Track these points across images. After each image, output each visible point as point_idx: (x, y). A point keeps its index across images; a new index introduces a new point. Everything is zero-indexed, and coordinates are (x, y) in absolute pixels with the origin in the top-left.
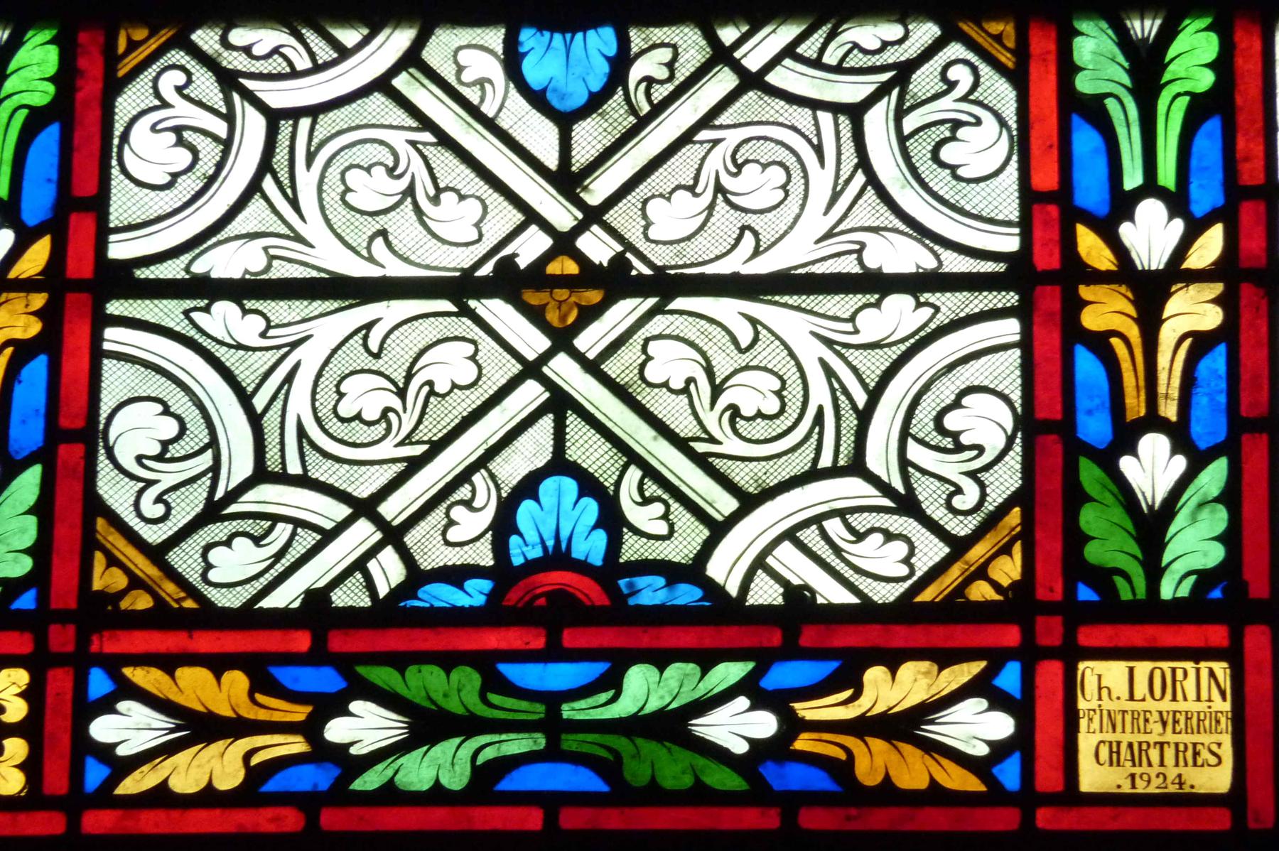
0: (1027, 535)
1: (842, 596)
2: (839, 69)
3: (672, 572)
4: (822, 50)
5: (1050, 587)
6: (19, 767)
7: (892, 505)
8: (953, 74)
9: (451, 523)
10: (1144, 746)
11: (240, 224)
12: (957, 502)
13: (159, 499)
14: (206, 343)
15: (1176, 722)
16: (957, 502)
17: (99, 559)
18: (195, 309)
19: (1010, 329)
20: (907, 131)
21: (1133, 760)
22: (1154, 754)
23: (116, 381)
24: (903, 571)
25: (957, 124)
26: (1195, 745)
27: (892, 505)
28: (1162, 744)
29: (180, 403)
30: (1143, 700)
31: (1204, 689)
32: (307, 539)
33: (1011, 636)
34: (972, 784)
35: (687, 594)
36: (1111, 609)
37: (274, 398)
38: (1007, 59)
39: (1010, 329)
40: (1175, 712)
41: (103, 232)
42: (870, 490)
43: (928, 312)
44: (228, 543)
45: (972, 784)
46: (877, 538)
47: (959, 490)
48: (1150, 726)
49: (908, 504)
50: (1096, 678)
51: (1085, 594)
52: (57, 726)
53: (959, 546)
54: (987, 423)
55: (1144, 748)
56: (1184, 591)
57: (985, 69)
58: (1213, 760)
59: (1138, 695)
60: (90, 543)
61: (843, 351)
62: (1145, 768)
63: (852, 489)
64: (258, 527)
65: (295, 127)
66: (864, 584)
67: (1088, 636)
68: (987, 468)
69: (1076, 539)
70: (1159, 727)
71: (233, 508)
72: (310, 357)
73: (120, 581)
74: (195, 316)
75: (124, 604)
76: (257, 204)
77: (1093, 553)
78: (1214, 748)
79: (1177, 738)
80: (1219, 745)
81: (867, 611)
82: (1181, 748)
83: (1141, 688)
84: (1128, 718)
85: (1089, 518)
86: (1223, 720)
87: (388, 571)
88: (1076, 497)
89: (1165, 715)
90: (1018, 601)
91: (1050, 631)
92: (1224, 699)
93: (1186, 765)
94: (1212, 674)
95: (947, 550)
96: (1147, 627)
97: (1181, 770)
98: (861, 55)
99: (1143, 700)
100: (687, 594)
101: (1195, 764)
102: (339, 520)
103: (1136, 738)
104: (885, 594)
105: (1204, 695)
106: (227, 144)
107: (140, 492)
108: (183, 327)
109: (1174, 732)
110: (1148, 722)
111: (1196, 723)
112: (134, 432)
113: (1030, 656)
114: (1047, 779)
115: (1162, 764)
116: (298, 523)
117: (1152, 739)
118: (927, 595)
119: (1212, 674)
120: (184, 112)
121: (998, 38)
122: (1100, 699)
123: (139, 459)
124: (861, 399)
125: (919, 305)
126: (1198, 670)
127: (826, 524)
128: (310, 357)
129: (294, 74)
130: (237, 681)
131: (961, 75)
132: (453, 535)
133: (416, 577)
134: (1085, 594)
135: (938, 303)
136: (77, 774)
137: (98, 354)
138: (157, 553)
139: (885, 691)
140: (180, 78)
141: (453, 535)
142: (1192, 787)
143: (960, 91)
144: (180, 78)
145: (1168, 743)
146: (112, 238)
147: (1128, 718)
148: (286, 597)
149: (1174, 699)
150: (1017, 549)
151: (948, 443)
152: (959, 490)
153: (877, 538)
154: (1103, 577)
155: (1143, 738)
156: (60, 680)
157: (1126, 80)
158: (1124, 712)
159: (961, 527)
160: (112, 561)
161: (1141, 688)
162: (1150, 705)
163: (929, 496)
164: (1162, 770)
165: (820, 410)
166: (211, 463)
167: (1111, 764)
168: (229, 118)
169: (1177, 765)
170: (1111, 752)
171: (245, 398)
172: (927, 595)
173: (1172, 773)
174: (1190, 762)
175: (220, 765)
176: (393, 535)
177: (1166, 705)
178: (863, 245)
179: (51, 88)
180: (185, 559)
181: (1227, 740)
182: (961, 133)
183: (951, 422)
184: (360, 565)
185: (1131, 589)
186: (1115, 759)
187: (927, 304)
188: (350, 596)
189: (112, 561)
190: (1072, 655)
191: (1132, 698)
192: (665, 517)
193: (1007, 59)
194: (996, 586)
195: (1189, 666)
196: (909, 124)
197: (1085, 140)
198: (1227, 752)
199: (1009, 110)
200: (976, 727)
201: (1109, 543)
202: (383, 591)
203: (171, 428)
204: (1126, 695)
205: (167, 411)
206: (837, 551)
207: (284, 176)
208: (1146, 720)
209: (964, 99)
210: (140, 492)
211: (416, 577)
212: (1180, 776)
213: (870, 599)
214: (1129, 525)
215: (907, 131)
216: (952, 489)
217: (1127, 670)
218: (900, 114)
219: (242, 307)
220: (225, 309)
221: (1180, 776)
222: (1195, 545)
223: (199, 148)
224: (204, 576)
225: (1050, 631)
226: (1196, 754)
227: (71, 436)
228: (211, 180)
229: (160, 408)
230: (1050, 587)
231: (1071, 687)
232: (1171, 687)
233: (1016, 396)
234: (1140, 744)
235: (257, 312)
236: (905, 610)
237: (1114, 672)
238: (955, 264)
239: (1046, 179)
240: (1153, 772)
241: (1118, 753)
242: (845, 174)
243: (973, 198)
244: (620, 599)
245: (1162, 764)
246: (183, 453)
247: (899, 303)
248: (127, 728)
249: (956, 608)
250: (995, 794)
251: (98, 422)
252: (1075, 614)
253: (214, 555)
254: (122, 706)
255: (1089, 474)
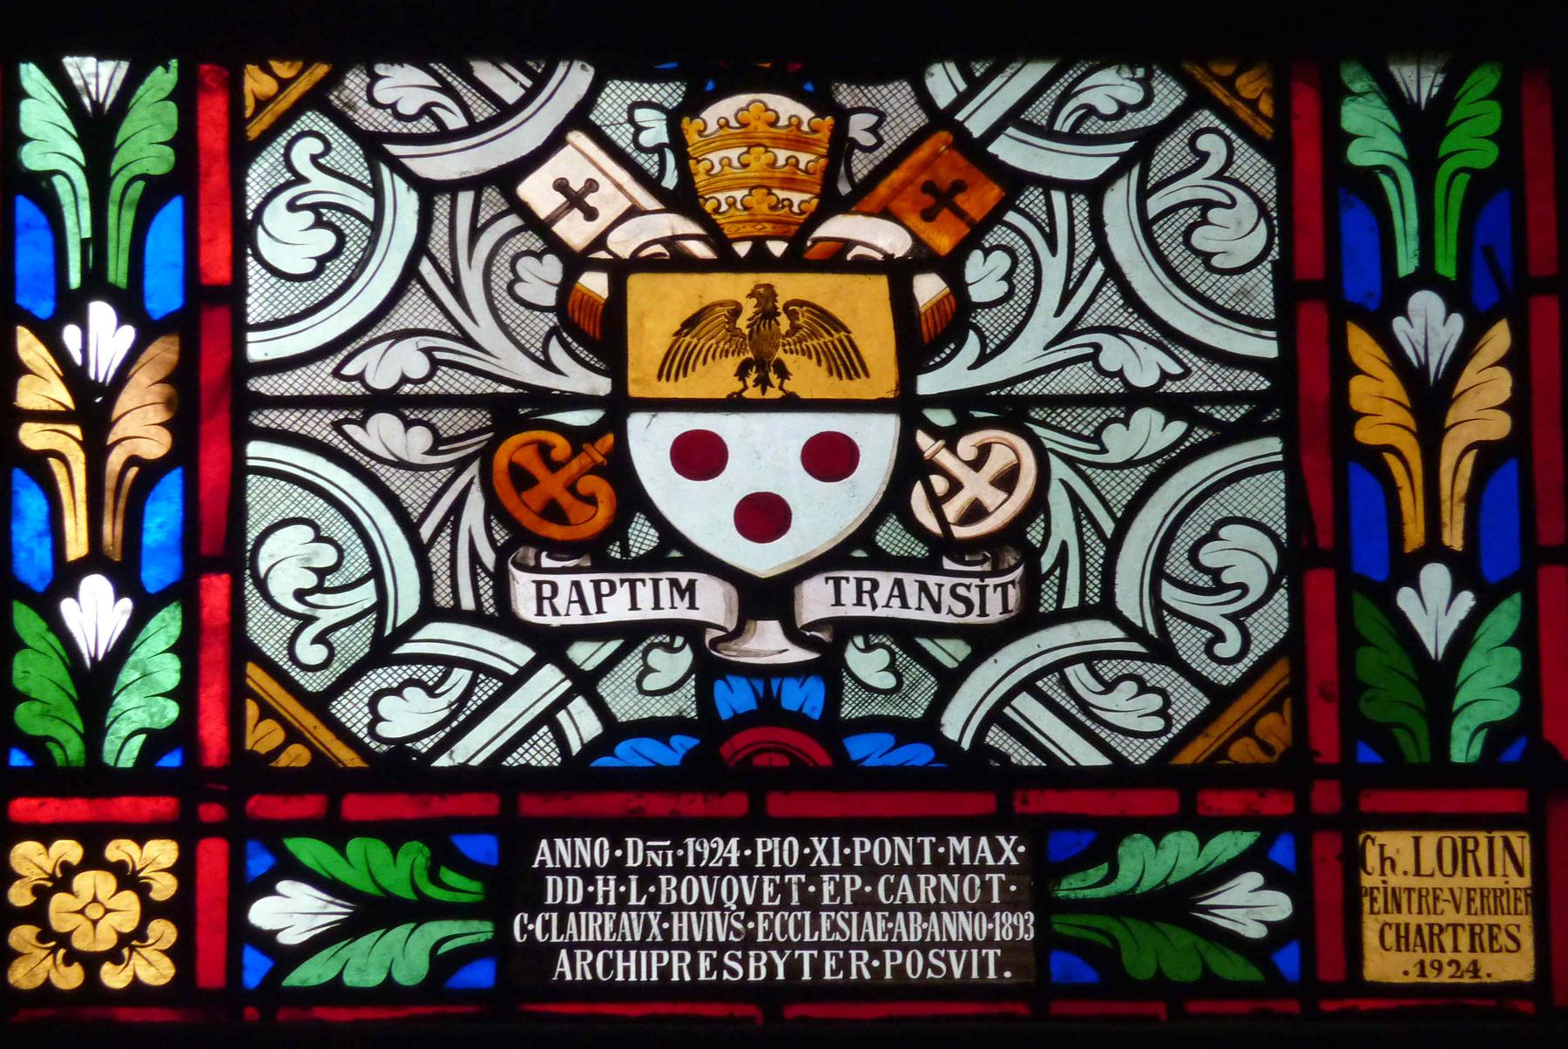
0: (1296, 690)
1: (1090, 757)
2: (451, 663)
3: (903, 730)
4: (473, 683)
5: (1326, 743)
6: (166, 952)
7: (1142, 650)
8: (1204, 143)
9: (647, 670)
10: (1436, 930)
11: (402, 317)
12: (318, 147)
13: (1204, 157)
14: (364, 460)
15: (1470, 900)
16: (318, 147)
17: (252, 709)
18: (347, 421)
19: (259, 348)
20: (1152, 214)
21: (1423, 946)
22: (1447, 939)
23: (1262, 296)
24: (1157, 724)
25: (1207, 205)
26: (1491, 927)
27: (1142, 650)
28: (1455, 926)
29: (342, 531)
30: (1432, 875)
31: (1504, 864)
32: (488, 688)
33: (1279, 804)
34: (1253, 974)
35: (919, 755)
36: (1396, 773)
37: (1084, 274)
38: (1265, 130)
39: (259, 348)
40: (1469, 890)
41: (239, 327)
42: (412, 164)
43: (349, 370)
44: (397, 692)
45: (1253, 974)
46: (1130, 687)
47: (314, 159)
48: (1441, 905)
49: (1162, 651)
50: (1377, 849)
51: (1366, 755)
52: (212, 911)
53: (1220, 697)
54: (288, 240)
55: (1436, 931)
56: (1476, 750)
57: (1238, 143)
58: (1512, 946)
59: (1425, 869)
60: (239, 692)
61: (1089, 471)
62: (1437, 955)
63: (1100, 631)
64: (430, 674)
65: (1083, 594)
66: (1116, 741)
67: (1371, 802)
68: (287, 185)
69: (1351, 688)
70: (1450, 907)
71: (406, 649)
72: (1044, 324)
73: (279, 736)
74: (348, 428)
75: (283, 761)
76: (416, 294)
77: (1372, 710)
78: (1513, 930)
79: (1473, 920)
80: (1518, 927)
81: (1120, 772)
82: (1477, 930)
83: (1429, 861)
84: (1415, 896)
85: (1368, 663)
86: (1521, 895)
87: (582, 724)
88: (1350, 640)
89: (1457, 894)
90: (1293, 768)
91: (1326, 796)
92: (1520, 872)
93: (1483, 950)
94: (1507, 845)
95: (1206, 701)
96: (1438, 795)
97: (1478, 956)
98: (425, 678)
99: (1432, 875)
100: (919, 755)
101: (1492, 950)
102: (522, 664)
103: (1424, 920)
104: (1139, 753)
105: (1498, 869)
106: (376, 226)
107: (1229, 162)
108: (336, 441)
109: (1469, 913)
110: (1437, 903)
111: (1496, 899)
112: (286, 561)
113: (1303, 825)
114: (1330, 969)
115: (1456, 950)
116: (477, 668)
117: (1443, 920)
118: (1188, 756)
119: (1507, 845)
120: (1211, 611)
121: (1252, 104)
122: (1383, 873)
123: (300, 595)
124: (1108, 527)
125: (360, 377)
126: (1491, 841)
127: (1069, 671)
128: (1044, 324)
129: (1089, 659)
130: (415, 854)
131: (311, 653)
132: (650, 683)
133: (615, 732)
134: (1366, 755)
135: (335, 382)
136: (235, 966)
137: (239, 471)
138: (319, 704)
139: (1147, 863)
140: (316, 146)
141: (650, 683)
142: (1489, 975)
143: (1212, 166)
144: (316, 146)
145: (1463, 926)
146: (251, 336)
147: (1415, 896)
148: (472, 748)
149: (1465, 874)
150: (1288, 702)
151: (1205, 581)
152: (1219, 636)
153: (1130, 687)
154: (1382, 736)
155: (1433, 919)
156: (213, 853)
157: (1400, 149)
158: (1409, 890)
159: (1227, 676)
160: (267, 712)
161: (1429, 861)
162: (1438, 881)
163: (1188, 643)
164: (1456, 956)
165: (1064, 546)
166: (373, 599)
167: (1399, 950)
168: (377, 192)
169: (1473, 950)
170: (1398, 937)
171: (410, 528)
172: (1188, 756)
173: (1465, 958)
174: (1486, 944)
175: (401, 955)
176: (585, 684)
177: (1458, 882)
178: (1097, 348)
179: (169, 151)
180: (1169, 95)
181: (1526, 922)
182: (1214, 214)
183: (327, 240)
184: (548, 718)
185: (1415, 750)
186: (1402, 942)
187: (349, 379)
188: (540, 753)
189: (267, 712)
190: (1353, 825)
191: (1418, 873)
192: (639, 129)
193: (1265, 130)
194: (1266, 747)
195: (1482, 837)
196: (1155, 205)
197: (1355, 219)
198: (1527, 940)
199: (1266, 185)
200: (1251, 906)
201: (1391, 698)
202: (576, 747)
203: (1200, 239)
204: (1411, 868)
205: (1206, 257)
206: (1084, 705)
207: (1091, 537)
208: (1436, 898)
209: (1219, 176)
210: (1229, 162)
211: (615, 732)
212: (1475, 963)
213: (1125, 760)
214: (1408, 669)
215: (1152, 214)
216: (1209, 635)
217: (1412, 842)
218: (1143, 194)
219: (403, 418)
220: (1144, 378)
221: (1475, 963)
222: (1488, 691)
223: (1187, 563)
224: (372, 727)
225: (1326, 796)
226: (1492, 938)
227: (215, 566)
228: (362, 265)
229: (1216, 262)
230: (1326, 743)
231: (1355, 860)
232: (1462, 858)
233: (253, 267)
234: (1431, 926)
235: (419, 422)
236: (1160, 770)
237: (1397, 842)
238: (317, 424)
239: (1310, 266)
240: (1445, 958)
241: (1407, 937)
242: (1079, 262)
243: (1224, 290)
244: (841, 755)
245: (1456, 950)
246: (337, 584)
247: (382, 380)
248: (292, 912)
249: (1217, 772)
250: (1274, 983)
251: (245, 551)
252: (1353, 778)
253: (385, 705)
254: (283, 886)
255: (1366, 614)
